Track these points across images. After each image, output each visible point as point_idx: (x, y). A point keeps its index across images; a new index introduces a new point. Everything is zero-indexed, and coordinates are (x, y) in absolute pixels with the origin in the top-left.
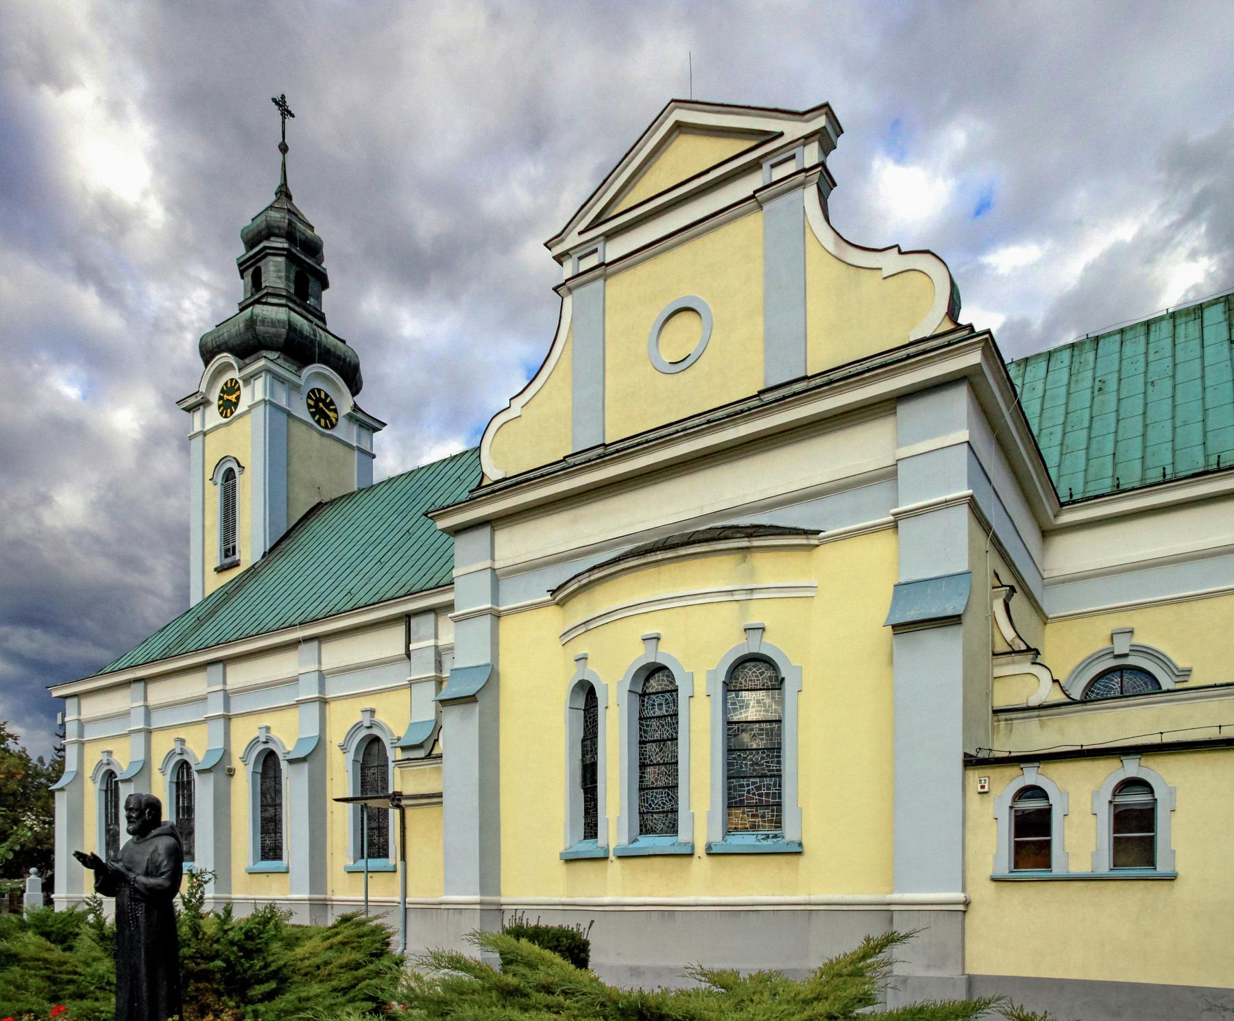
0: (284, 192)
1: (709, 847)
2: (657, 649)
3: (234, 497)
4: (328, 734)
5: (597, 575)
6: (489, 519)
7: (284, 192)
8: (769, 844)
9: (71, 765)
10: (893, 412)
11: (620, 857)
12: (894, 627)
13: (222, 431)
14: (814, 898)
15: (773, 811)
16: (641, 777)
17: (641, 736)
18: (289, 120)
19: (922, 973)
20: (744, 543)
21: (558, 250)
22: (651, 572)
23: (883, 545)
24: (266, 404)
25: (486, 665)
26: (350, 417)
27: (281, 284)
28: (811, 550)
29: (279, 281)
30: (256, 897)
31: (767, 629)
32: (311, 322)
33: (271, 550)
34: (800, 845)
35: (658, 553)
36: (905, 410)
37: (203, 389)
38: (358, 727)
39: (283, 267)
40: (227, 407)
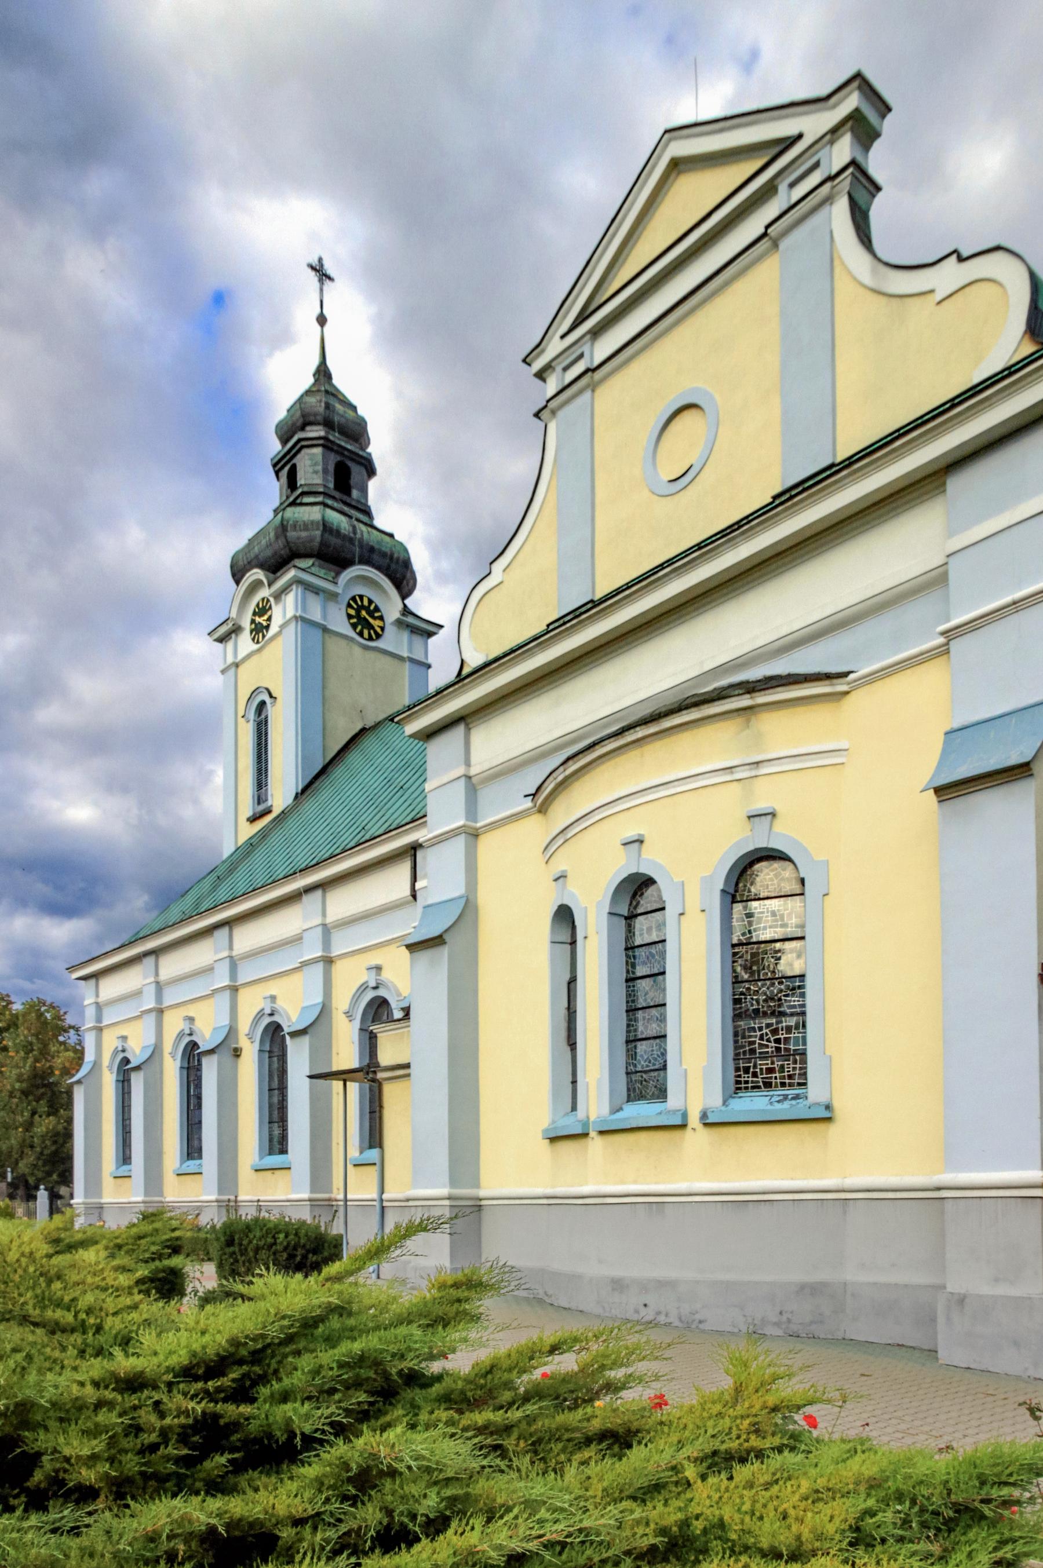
0: (323, 373)
1: (704, 1115)
2: (640, 855)
3: (266, 734)
4: (334, 1001)
5: (573, 767)
6: (463, 713)
7: (323, 373)
8: (784, 1109)
9: (89, 1057)
10: (941, 488)
11: (601, 1133)
12: (939, 791)
13: (255, 659)
14: (850, 1182)
15: (795, 1062)
16: (628, 1026)
17: (628, 972)
18: (328, 284)
19: (986, 1290)
20: (745, 701)
21: (538, 365)
22: (633, 756)
23: (934, 675)
24: (297, 622)
25: (460, 897)
26: (399, 623)
27: (318, 480)
28: (839, 700)
29: (315, 476)
30: (261, 1198)
31: (779, 816)
32: (350, 517)
33: (304, 791)
34: (828, 1107)
35: (638, 729)
36: (957, 484)
37: (234, 615)
38: (364, 988)
39: (320, 458)
40: (259, 630)
